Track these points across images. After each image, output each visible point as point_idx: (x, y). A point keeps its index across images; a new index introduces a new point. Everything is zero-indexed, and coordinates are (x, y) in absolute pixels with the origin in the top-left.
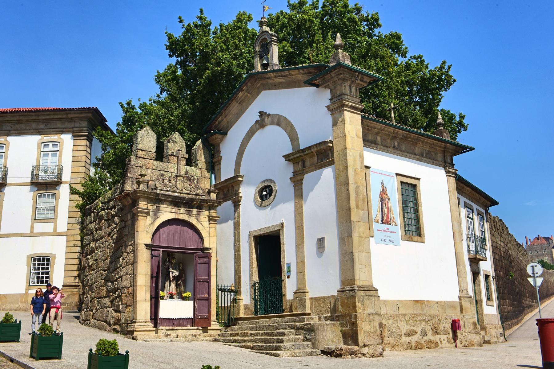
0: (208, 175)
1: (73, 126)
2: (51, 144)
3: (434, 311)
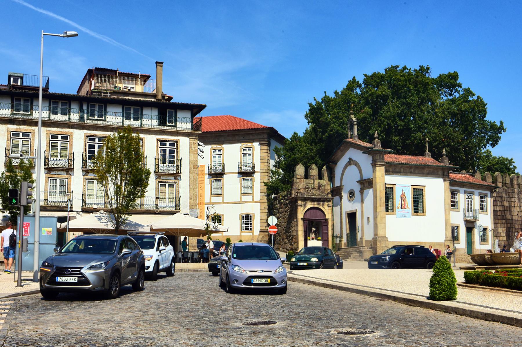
0: (329, 183)
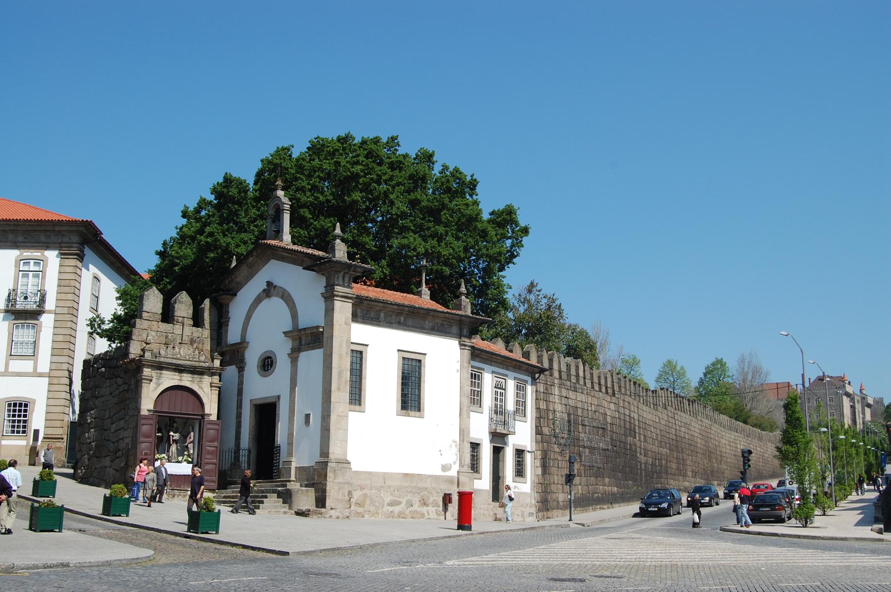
1: (60, 241)
2: (32, 262)
3: (428, 484)
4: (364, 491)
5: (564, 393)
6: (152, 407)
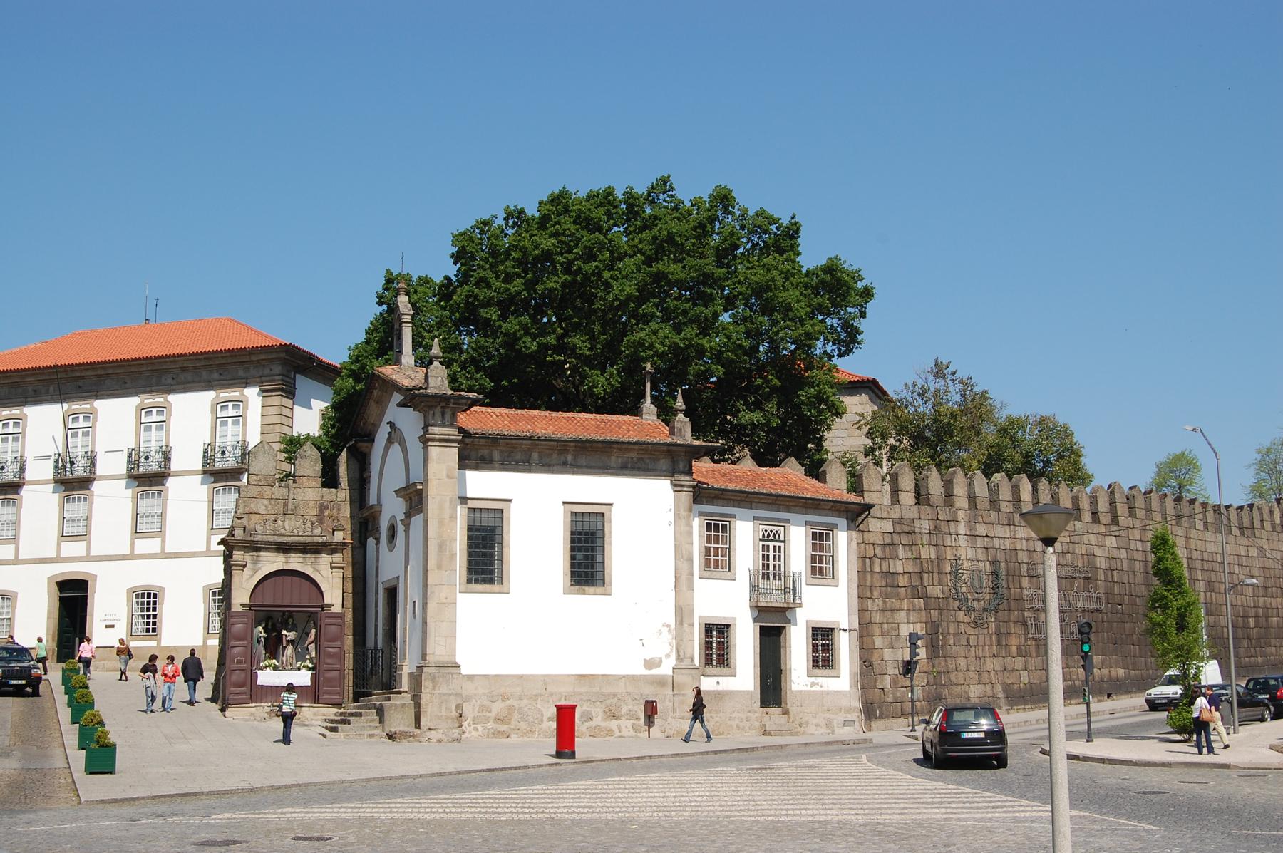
3: (621, 688)
4: (509, 702)
5: (981, 529)
6: (247, 601)
